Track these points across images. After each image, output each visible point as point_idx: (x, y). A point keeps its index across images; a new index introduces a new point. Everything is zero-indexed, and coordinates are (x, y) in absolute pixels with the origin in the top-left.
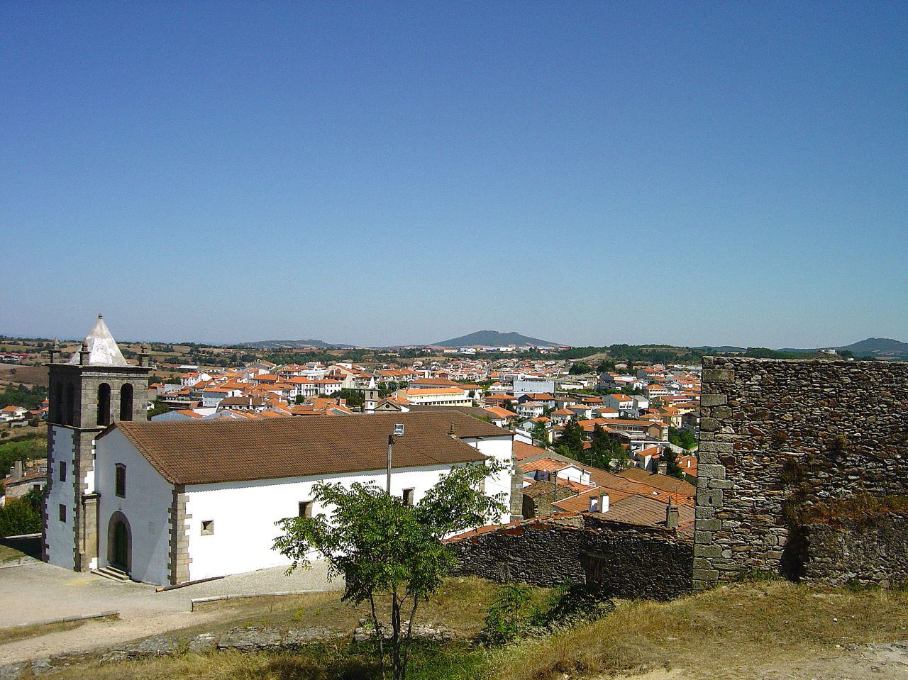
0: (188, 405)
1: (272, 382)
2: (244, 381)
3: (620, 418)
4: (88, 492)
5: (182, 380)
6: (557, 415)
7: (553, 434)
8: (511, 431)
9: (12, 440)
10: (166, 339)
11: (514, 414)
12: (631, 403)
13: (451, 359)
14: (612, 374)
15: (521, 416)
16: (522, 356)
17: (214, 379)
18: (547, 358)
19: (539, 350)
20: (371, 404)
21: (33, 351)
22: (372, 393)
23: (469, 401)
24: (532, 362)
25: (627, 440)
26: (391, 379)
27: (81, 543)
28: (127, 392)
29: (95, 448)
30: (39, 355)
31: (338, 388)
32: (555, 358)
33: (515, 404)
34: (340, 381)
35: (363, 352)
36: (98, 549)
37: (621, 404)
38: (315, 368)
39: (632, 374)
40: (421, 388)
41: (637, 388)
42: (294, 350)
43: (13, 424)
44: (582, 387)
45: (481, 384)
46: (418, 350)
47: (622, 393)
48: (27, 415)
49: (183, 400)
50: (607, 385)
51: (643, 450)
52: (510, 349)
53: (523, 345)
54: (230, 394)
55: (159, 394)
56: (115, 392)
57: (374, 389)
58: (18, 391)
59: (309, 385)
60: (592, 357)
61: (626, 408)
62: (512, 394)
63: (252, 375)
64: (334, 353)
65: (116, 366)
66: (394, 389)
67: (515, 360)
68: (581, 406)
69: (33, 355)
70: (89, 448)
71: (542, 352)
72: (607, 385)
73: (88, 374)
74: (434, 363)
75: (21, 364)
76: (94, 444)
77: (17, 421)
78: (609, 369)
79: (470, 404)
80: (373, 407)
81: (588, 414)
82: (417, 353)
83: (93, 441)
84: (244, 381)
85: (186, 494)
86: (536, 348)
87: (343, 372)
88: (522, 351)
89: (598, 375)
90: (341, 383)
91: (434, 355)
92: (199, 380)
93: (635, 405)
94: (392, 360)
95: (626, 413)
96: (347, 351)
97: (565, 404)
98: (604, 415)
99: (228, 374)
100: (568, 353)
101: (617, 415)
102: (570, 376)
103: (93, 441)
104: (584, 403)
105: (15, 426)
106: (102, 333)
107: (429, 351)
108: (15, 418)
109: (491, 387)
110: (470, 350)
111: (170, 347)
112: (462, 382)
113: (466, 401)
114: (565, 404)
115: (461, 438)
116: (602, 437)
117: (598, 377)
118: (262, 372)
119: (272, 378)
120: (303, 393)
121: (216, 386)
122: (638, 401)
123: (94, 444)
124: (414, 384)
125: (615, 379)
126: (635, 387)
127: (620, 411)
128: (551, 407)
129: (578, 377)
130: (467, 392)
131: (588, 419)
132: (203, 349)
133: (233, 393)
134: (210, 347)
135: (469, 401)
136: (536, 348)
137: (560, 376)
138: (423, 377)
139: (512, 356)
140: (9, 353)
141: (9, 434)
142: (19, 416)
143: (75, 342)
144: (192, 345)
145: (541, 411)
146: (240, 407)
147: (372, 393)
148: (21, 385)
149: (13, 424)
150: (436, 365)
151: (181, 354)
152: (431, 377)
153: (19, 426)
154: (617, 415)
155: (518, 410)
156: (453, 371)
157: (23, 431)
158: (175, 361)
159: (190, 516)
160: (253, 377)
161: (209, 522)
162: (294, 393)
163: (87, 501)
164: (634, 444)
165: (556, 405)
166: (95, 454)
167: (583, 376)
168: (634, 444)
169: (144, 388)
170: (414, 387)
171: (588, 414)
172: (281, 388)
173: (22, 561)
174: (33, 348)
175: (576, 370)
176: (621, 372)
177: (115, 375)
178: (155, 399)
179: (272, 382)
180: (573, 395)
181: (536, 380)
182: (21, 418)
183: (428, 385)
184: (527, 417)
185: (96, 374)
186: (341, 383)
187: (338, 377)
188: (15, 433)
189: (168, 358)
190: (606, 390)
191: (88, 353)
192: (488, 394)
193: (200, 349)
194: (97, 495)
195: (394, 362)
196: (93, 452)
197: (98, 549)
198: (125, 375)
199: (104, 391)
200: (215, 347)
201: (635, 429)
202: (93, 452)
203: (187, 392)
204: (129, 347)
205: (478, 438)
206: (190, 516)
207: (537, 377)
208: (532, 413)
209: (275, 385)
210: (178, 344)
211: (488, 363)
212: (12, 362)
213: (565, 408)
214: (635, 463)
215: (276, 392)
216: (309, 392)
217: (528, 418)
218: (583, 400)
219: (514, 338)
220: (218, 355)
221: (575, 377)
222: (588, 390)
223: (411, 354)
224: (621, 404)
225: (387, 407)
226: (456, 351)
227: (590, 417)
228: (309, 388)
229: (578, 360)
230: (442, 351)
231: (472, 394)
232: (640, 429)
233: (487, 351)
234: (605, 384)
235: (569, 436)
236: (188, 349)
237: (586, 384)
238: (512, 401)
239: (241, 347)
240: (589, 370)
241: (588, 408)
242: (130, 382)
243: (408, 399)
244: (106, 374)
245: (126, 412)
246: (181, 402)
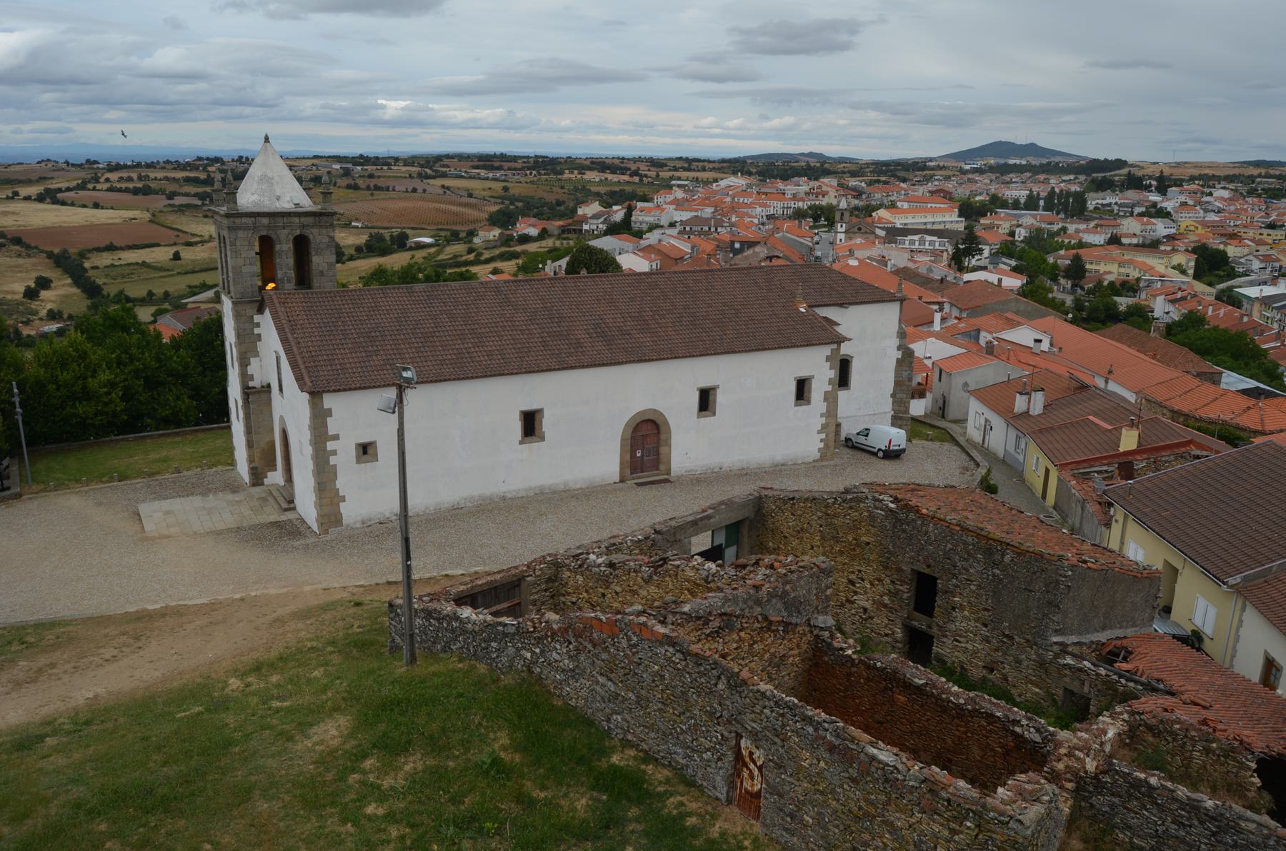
28: (301, 245)
56: (285, 249)
159: (336, 437)
206: (336, 437)
215: (745, 210)
219: (1032, 149)
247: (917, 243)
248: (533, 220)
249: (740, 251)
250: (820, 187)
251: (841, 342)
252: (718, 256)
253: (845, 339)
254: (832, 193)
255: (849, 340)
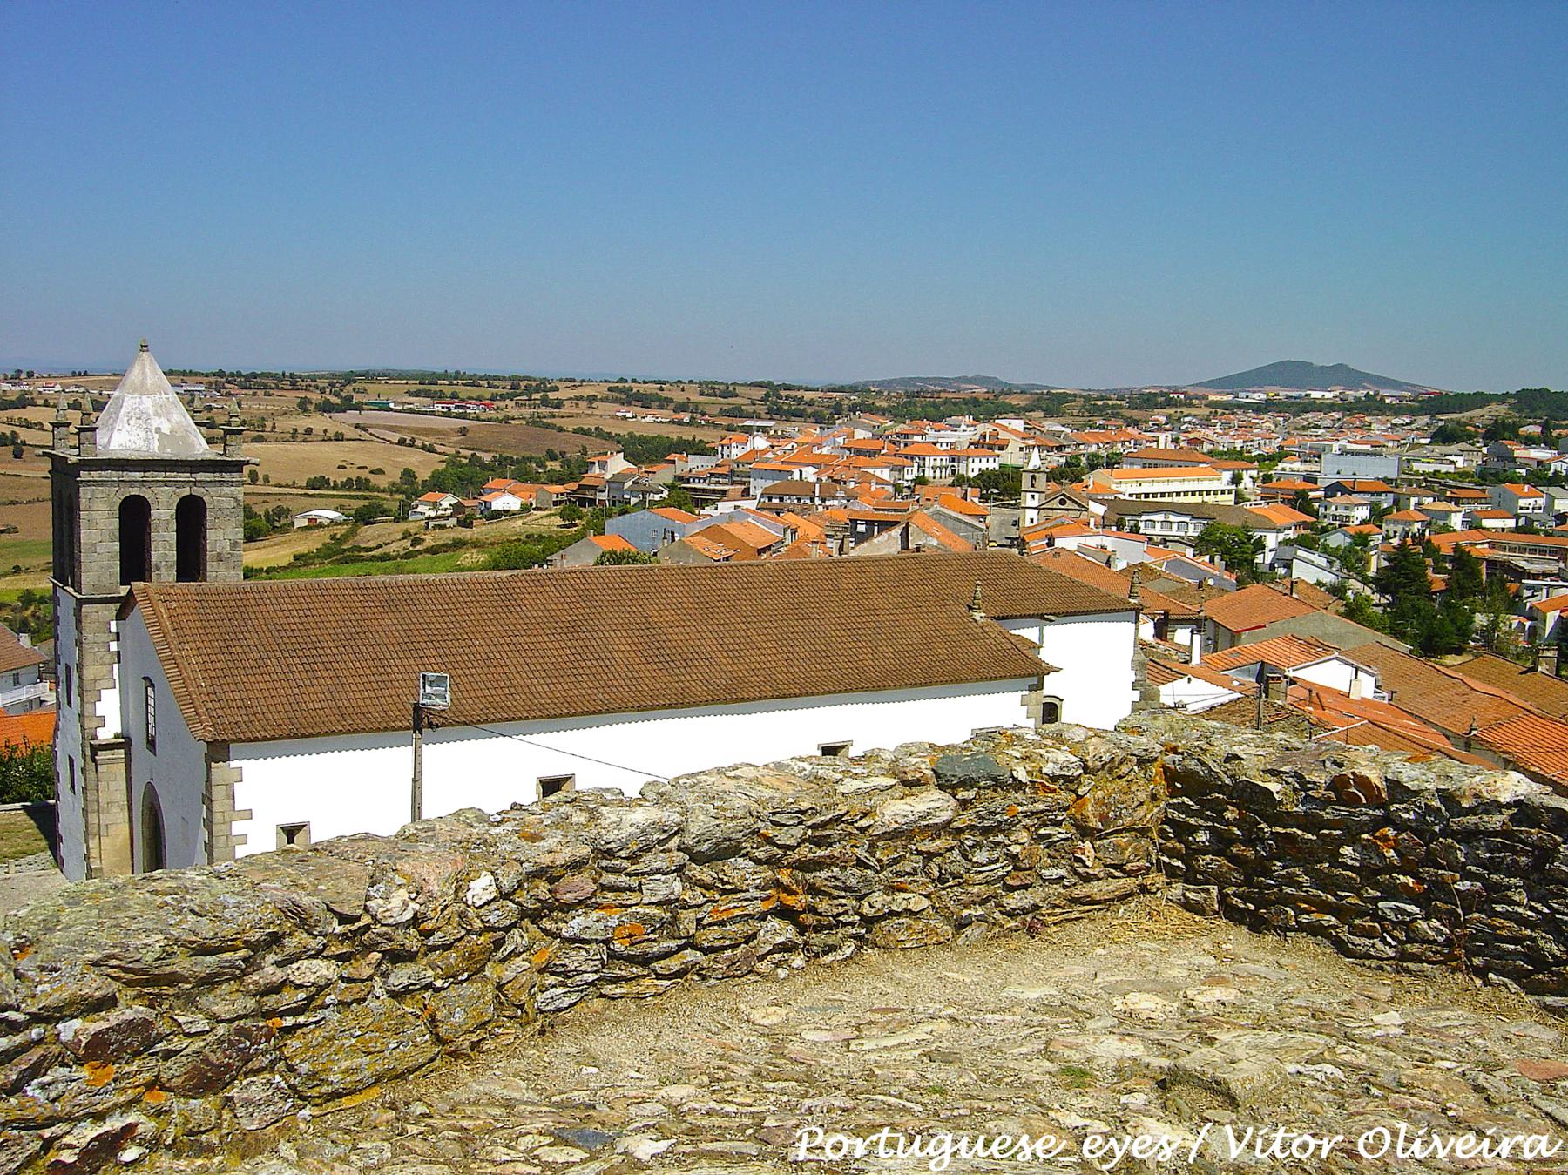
0: (724, 492)
1: (873, 453)
2: (825, 451)
3: (1517, 530)
4: (105, 735)
5: (720, 448)
6: (1396, 522)
7: (1378, 558)
8: (1132, 601)
9: (427, 551)
10: (725, 374)
11: (1309, 519)
12: (1541, 502)
13: (1220, 412)
14: (1511, 445)
15: (1326, 522)
16: (1349, 408)
17: (773, 447)
18: (1396, 411)
19: (1383, 399)
20: (1033, 496)
21: (503, 397)
22: (1033, 478)
23: (1230, 492)
24: (1367, 419)
25: (1520, 574)
26: (1094, 449)
27: (93, 844)
28: (191, 515)
29: (118, 637)
30: (511, 403)
31: (993, 465)
32: (1411, 412)
33: (1318, 499)
34: (997, 452)
35: (1064, 398)
36: (132, 857)
37: (1522, 503)
38: (963, 427)
39: (1550, 444)
40: (1144, 466)
41: (1556, 472)
42: (942, 395)
43: (431, 524)
44: (1451, 469)
45: (1261, 459)
46: (1162, 394)
47: (1526, 481)
48: (457, 508)
49: (718, 483)
50: (1500, 465)
51: (1544, 599)
52: (1329, 395)
53: (1356, 388)
54: (796, 476)
55: (679, 473)
56: (163, 518)
57: (1038, 470)
58: (466, 465)
59: (939, 458)
60: (1479, 411)
61: (1530, 511)
62: (1314, 481)
63: (840, 440)
64: (1014, 401)
65: (167, 456)
66: (1093, 467)
67: (1336, 415)
68: (1444, 506)
69: (502, 404)
70: (104, 637)
71: (1388, 401)
72: (1500, 465)
73: (95, 475)
74: (1187, 419)
75: (478, 419)
76: (114, 629)
77: (442, 517)
78: (1506, 434)
79: (1229, 499)
80: (1035, 503)
81: (1456, 521)
82: (1160, 399)
83: (113, 624)
84: (825, 451)
85: (234, 764)
86: (1377, 394)
87: (1002, 435)
88: (1351, 399)
89: (1485, 446)
90: (998, 456)
91: (1191, 405)
92: (749, 448)
93: (1549, 507)
94: (1115, 412)
95: (1529, 521)
96: (1036, 396)
97: (1414, 500)
98: (1486, 523)
99: (801, 438)
100: (1436, 404)
101: (1511, 523)
102: (1430, 447)
103: (113, 624)
104: (1449, 500)
105: (435, 527)
106: (143, 383)
107: (1182, 396)
108: (440, 513)
109: (1281, 465)
110: (1255, 396)
111: (731, 389)
112: (1218, 457)
113: (1223, 492)
114: (1414, 500)
115: (997, 619)
116: (1469, 570)
117: (1485, 450)
118: (860, 434)
119: (876, 445)
120: (929, 474)
121: (775, 459)
122: (1554, 498)
123: (114, 629)
124: (1132, 459)
125: (1517, 454)
126: (1552, 471)
127: (1517, 517)
128: (1385, 506)
129: (1445, 449)
130: (1227, 476)
131: (1454, 530)
132: (788, 392)
133: (801, 472)
134: (799, 388)
135: (1230, 492)
136: (1377, 394)
137: (1413, 446)
138: (1154, 445)
139: (1331, 407)
140: (463, 400)
141: (424, 540)
142: (445, 510)
143: (574, 381)
144: (768, 385)
145: (1364, 513)
146: (799, 500)
147: (1033, 478)
148: (473, 455)
149: (431, 524)
150: (1189, 422)
151: (749, 402)
152: (1171, 447)
153: (443, 527)
154: (1511, 523)
155: (1322, 510)
156: (1219, 435)
157: (447, 535)
158: (737, 413)
159: (248, 815)
160: (841, 444)
161: (300, 827)
162: (911, 473)
163: (101, 755)
164: (1529, 587)
165: (1396, 502)
166: (119, 652)
167: (1455, 448)
168: (1529, 587)
169: (233, 504)
170: (1132, 464)
171: (1456, 521)
172: (887, 465)
173: (12, 868)
174: (505, 391)
175: (1444, 436)
176: (1529, 441)
177: (161, 476)
178: (670, 481)
179: (873, 453)
180: (1430, 483)
181: (1365, 454)
182: (449, 512)
183: (1156, 462)
184: (1338, 523)
185: (114, 475)
186: (998, 456)
187: (992, 445)
188: (434, 539)
189: (726, 407)
190: (1495, 475)
191: (94, 429)
192: (1267, 479)
193: (783, 393)
194: (124, 742)
195: (1116, 415)
196: (114, 646)
197: (132, 857)
198: (185, 476)
199: (134, 515)
200: (807, 389)
201: (1542, 552)
202: (114, 646)
203: (724, 470)
204: (662, 389)
205: (1042, 618)
206: (248, 815)
207: (1368, 447)
208: (1347, 517)
209: (878, 459)
210: (745, 385)
211: (1285, 421)
212: (464, 416)
213: (1412, 508)
214: (1528, 624)
215: (871, 471)
216: (938, 471)
217: (1340, 526)
218: (1448, 494)
219: (1340, 374)
220: (811, 403)
221: (1440, 449)
222: (1463, 475)
223: (1148, 401)
224: (1522, 503)
225: (1062, 502)
226: (1230, 397)
227: (1458, 527)
228: (938, 464)
229: (1454, 416)
230: (1205, 397)
231: (1236, 480)
232: (1552, 553)
233: (1288, 397)
234: (1495, 464)
235: (1403, 567)
236: (762, 392)
237: (1460, 462)
238: (1312, 494)
239: (853, 389)
240: (1469, 437)
241: (1456, 508)
242: (198, 491)
243: (1113, 486)
244: (138, 475)
245: (191, 563)
246: (712, 487)
247: (1158, 526)
248: (513, 484)
249: (867, 536)
250: (995, 435)
251: (1044, 674)
252: (829, 545)
253: (1051, 670)
254: (1015, 444)
255: (1057, 670)
